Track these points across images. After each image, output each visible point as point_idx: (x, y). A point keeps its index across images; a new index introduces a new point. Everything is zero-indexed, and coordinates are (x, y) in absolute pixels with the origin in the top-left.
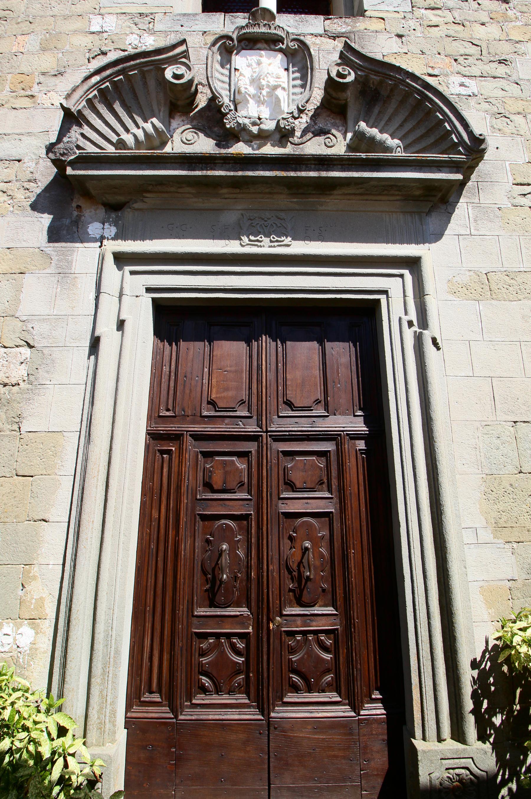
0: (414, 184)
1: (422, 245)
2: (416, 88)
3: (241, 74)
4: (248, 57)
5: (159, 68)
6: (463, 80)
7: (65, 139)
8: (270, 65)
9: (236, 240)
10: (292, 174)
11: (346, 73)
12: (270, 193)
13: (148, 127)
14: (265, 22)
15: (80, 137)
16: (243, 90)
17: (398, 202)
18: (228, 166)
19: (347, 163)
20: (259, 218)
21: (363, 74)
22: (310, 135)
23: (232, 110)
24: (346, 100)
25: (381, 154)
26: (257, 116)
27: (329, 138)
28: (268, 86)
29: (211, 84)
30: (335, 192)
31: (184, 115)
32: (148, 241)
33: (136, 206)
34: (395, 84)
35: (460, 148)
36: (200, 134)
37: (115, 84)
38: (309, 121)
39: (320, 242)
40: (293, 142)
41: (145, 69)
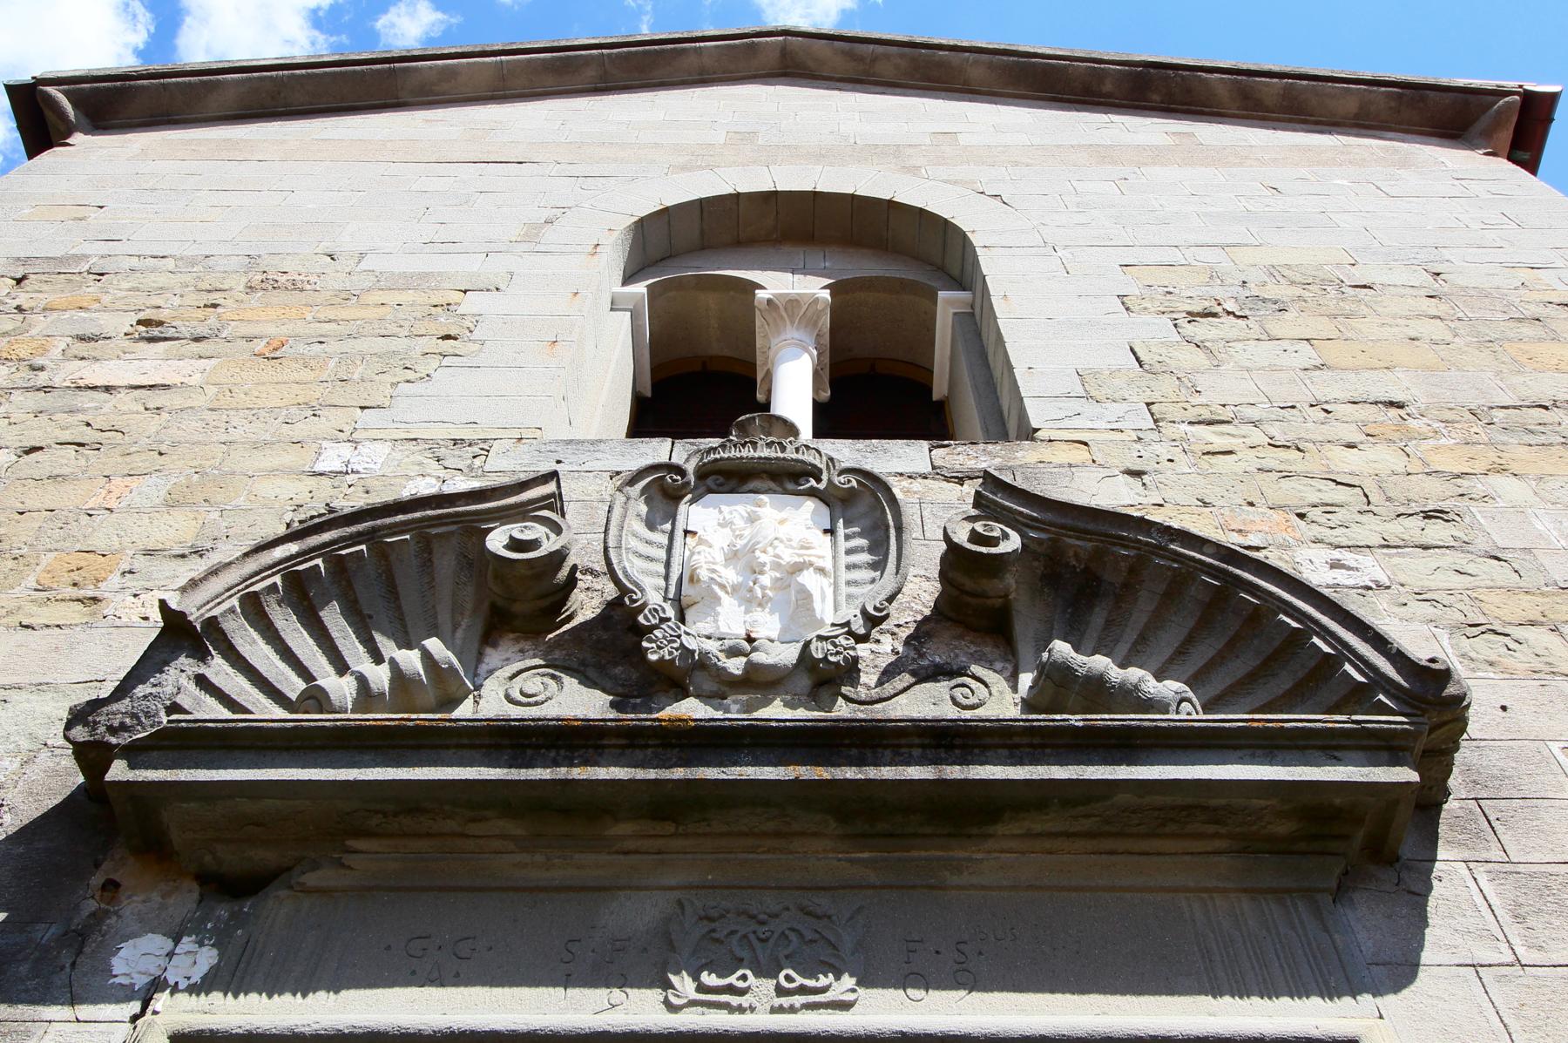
0: (1263, 803)
1: (1347, 1000)
2: (1200, 561)
3: (701, 542)
4: (723, 508)
5: (474, 529)
6: (1337, 554)
7: (140, 690)
8: (782, 522)
9: (650, 986)
10: (850, 773)
11: (996, 534)
12: (777, 834)
13: (411, 660)
14: (770, 439)
15: (191, 687)
16: (704, 574)
17: (1224, 858)
18: (639, 754)
19: (1025, 740)
20: (739, 914)
21: (1043, 536)
22: (907, 679)
23: (669, 619)
24: (1006, 596)
25: (1132, 716)
26: (743, 633)
27: (963, 685)
28: (777, 566)
29: (615, 561)
30: (1000, 829)
31: (526, 639)
32: (322, 994)
33: (311, 879)
34: (1139, 557)
35: (1381, 697)
36: (566, 679)
37: (339, 566)
38: (901, 649)
39: (962, 993)
40: (853, 696)
41: (434, 531)
